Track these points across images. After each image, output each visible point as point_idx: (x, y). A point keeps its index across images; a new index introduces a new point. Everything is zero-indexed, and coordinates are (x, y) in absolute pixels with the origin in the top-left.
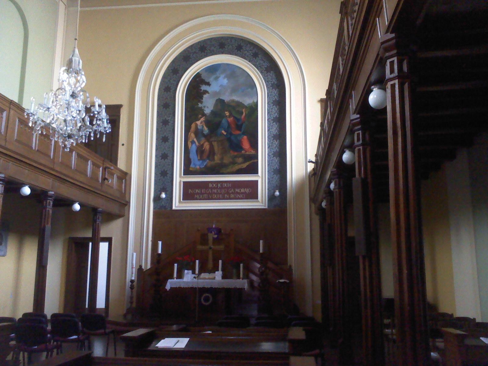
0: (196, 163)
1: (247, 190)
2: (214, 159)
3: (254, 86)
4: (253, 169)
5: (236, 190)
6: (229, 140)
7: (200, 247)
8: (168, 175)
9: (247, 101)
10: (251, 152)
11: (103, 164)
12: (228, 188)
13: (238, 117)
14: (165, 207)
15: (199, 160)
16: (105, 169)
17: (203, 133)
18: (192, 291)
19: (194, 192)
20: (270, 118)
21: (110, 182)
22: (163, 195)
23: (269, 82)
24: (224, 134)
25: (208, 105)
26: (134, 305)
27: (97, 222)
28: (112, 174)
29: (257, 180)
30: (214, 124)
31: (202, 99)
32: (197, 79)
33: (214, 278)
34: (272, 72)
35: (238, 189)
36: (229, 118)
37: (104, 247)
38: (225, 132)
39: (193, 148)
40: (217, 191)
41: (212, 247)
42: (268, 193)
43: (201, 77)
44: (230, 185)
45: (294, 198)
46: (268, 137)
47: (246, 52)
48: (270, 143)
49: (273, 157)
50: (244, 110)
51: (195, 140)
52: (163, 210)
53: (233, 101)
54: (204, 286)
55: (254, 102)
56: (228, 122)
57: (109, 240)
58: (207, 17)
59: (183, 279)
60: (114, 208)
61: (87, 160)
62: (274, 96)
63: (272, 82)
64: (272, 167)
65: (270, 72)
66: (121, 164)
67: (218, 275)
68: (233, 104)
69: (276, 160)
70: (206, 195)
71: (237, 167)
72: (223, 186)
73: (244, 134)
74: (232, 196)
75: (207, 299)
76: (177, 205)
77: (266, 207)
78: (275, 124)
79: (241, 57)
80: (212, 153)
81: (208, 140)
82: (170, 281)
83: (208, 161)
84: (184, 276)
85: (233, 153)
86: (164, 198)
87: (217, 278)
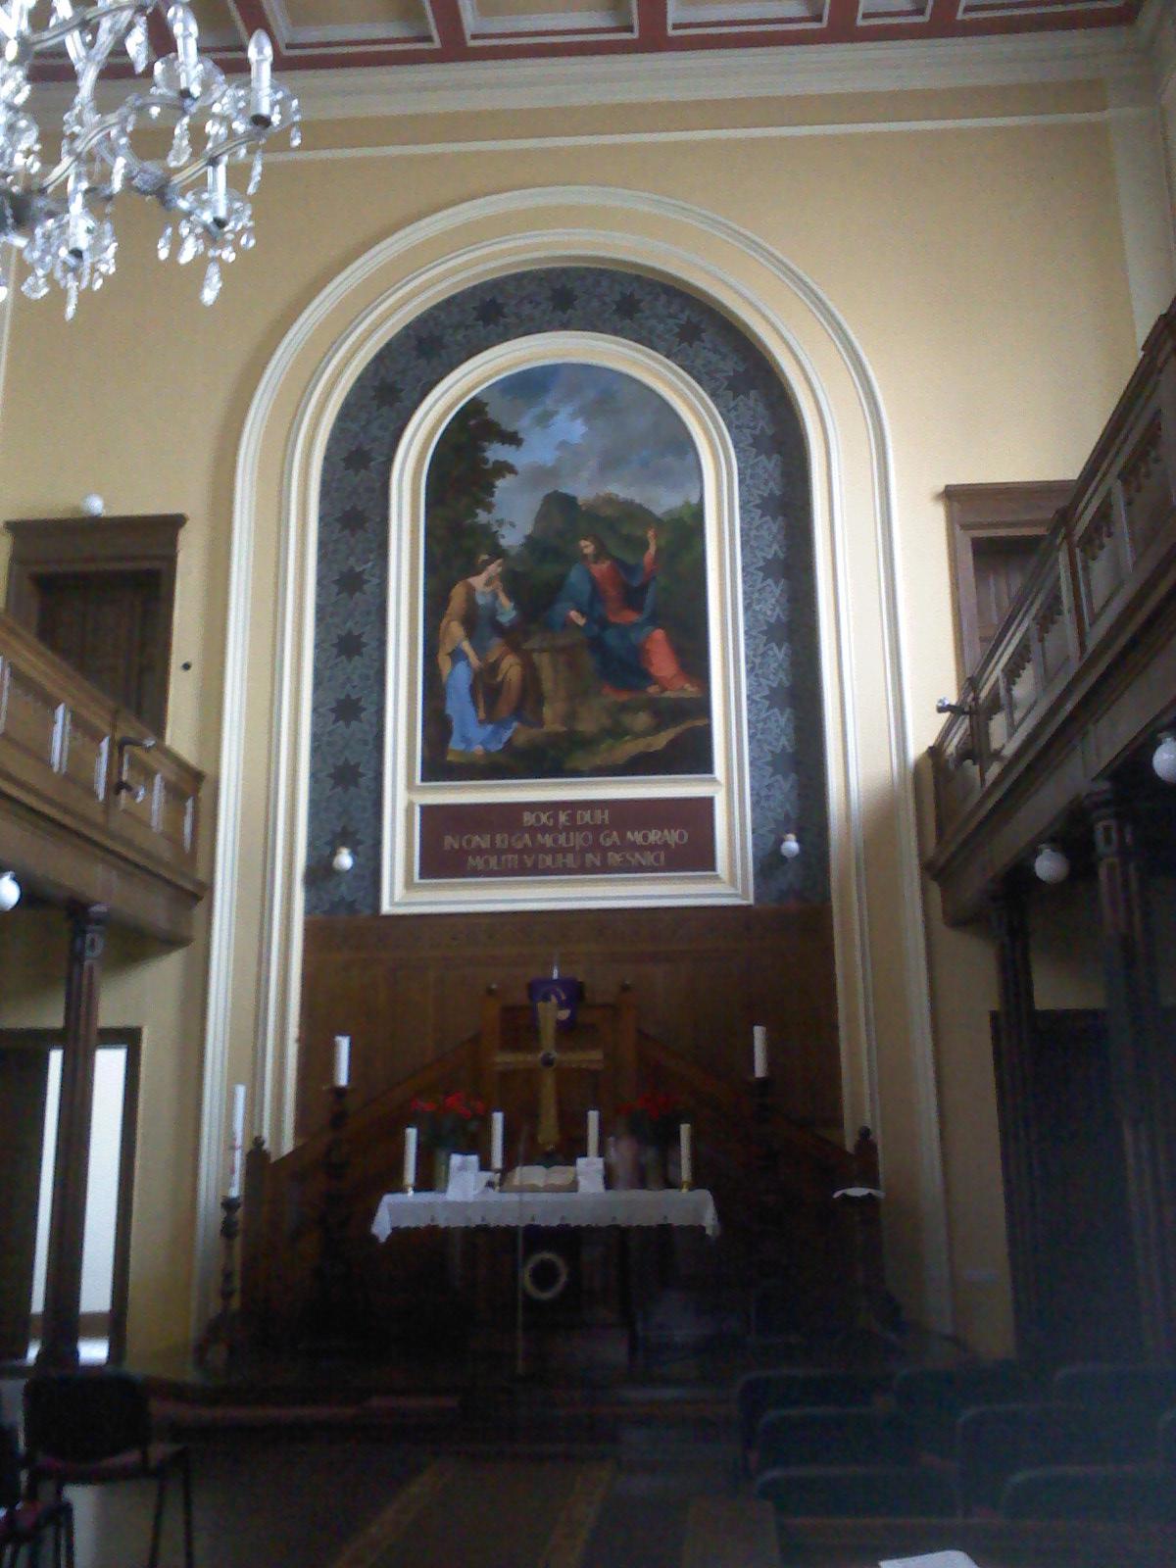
0: (472, 736)
1: (672, 837)
2: (540, 722)
3: (684, 445)
4: (694, 756)
5: (629, 834)
6: (597, 645)
7: (504, 1059)
8: (362, 781)
9: (664, 501)
10: (682, 689)
11: (114, 727)
12: (597, 829)
13: (629, 559)
14: (351, 907)
15: (481, 722)
16: (119, 747)
17: (497, 622)
18: (491, 1245)
19: (464, 844)
20: (753, 563)
21: (139, 800)
22: (345, 860)
23: (745, 430)
24: (575, 625)
25: (514, 515)
26: (236, 1303)
27: (86, 963)
28: (148, 774)
29: (711, 795)
30: (536, 588)
31: (492, 494)
32: (472, 422)
33: (573, 1186)
34: (753, 393)
35: (636, 833)
36: (596, 563)
37: (109, 1065)
38: (583, 614)
39: (459, 678)
40: (555, 840)
41: (555, 1055)
42: (755, 845)
43: (486, 413)
44: (606, 816)
45: (858, 859)
46: (746, 633)
47: (653, 322)
48: (754, 656)
49: (770, 708)
50: (650, 534)
51: (466, 646)
52: (344, 923)
53: (610, 500)
54: (666, 1217)
55: (687, 504)
56: (593, 580)
57: (128, 1038)
58: (509, 194)
59: (444, 1191)
60: (151, 908)
61: (51, 704)
62: (766, 483)
63: (755, 428)
64: (766, 747)
65: (747, 395)
66: (180, 735)
67: (589, 1170)
68: (609, 512)
69: (781, 719)
70: (510, 856)
71: (631, 748)
72: (576, 821)
73: (654, 620)
74: (614, 858)
75: (544, 1275)
76: (396, 900)
77: (751, 901)
78: (773, 584)
79: (637, 341)
80: (531, 695)
81: (515, 647)
82: (388, 1199)
83: (515, 724)
84: (447, 1181)
85: (612, 696)
86: (348, 871)
87: (585, 1188)
